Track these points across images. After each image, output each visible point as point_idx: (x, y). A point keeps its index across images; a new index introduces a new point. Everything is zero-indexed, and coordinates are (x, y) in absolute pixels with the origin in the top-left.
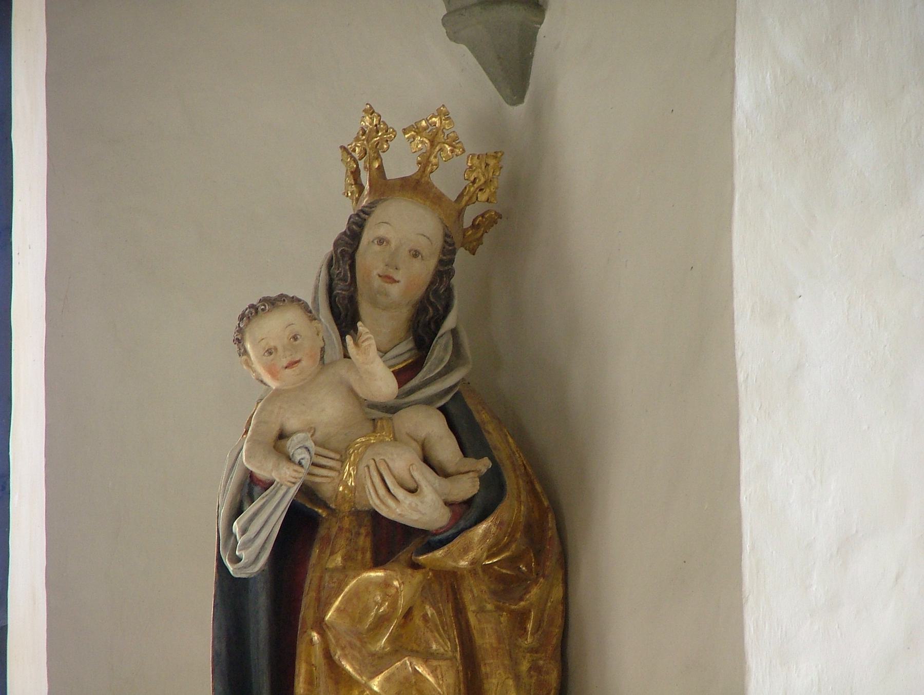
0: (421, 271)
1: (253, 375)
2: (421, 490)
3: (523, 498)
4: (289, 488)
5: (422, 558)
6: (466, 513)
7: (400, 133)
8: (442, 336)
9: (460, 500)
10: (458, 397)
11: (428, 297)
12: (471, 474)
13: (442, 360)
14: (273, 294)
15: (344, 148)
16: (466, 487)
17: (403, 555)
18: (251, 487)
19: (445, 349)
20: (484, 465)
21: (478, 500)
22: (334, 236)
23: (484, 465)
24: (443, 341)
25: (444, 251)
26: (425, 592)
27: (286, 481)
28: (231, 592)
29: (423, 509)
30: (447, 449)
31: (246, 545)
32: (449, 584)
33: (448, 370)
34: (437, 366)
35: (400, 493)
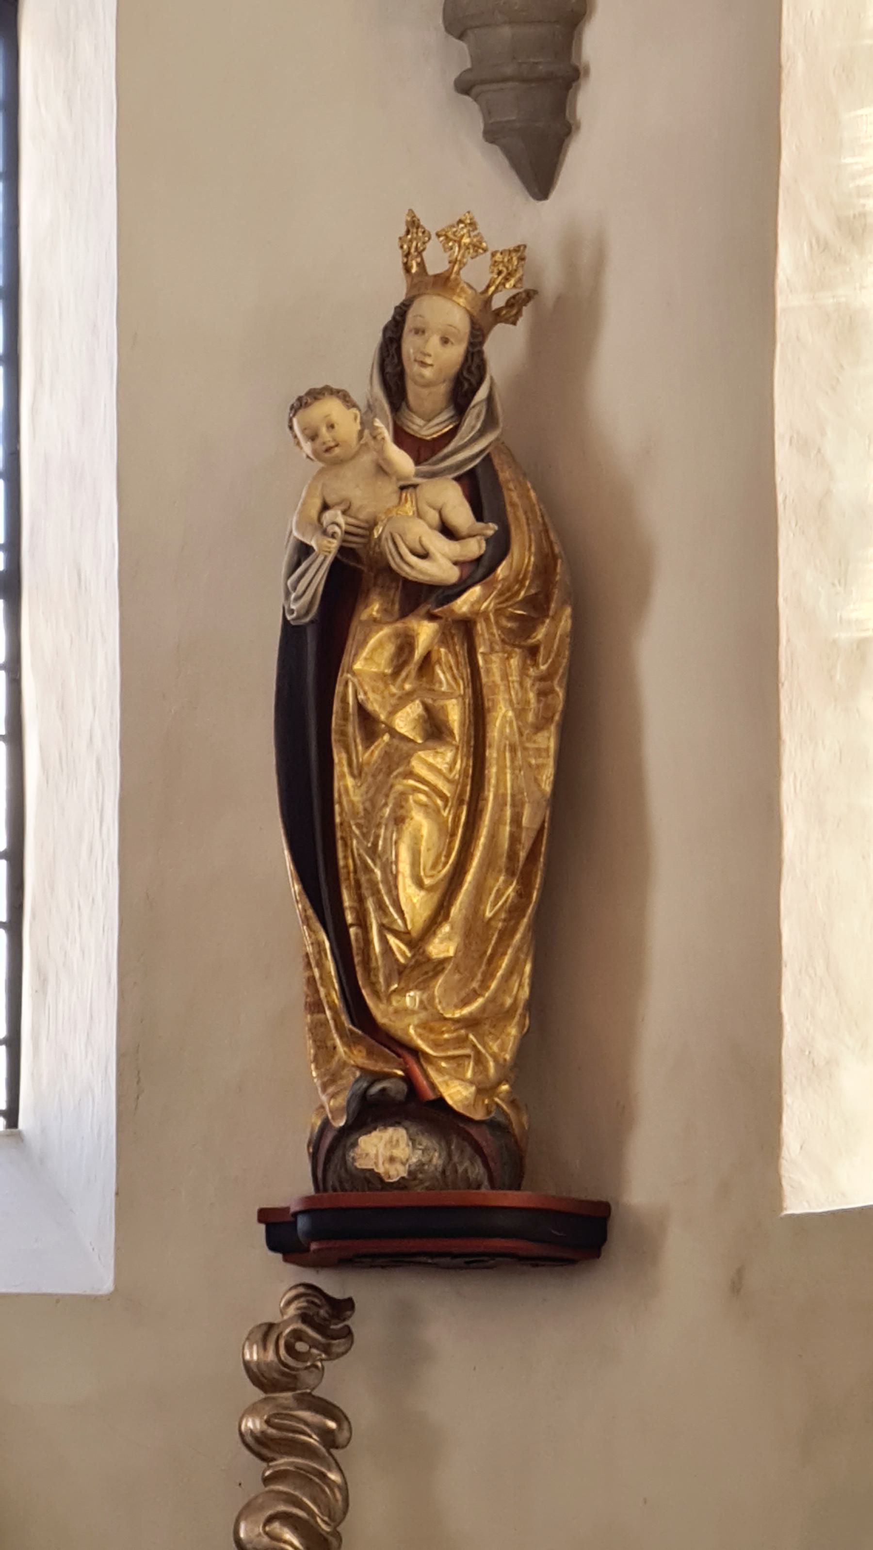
0: (456, 353)
1: (304, 456)
2: (431, 554)
3: (533, 549)
4: (326, 557)
5: (436, 611)
6: (477, 571)
7: (434, 236)
8: (474, 407)
9: (469, 559)
10: (488, 460)
11: (462, 374)
12: (479, 538)
13: (473, 427)
14: (319, 385)
15: (413, 224)
16: (474, 548)
17: (423, 610)
18: (303, 551)
19: (478, 416)
20: (491, 529)
21: (486, 558)
22: (382, 327)
23: (491, 529)
24: (475, 411)
25: (473, 335)
26: (444, 637)
27: (326, 549)
28: (291, 634)
29: (440, 565)
30: (461, 514)
31: (297, 599)
32: (465, 627)
33: (481, 433)
34: (470, 433)
35: (413, 560)
